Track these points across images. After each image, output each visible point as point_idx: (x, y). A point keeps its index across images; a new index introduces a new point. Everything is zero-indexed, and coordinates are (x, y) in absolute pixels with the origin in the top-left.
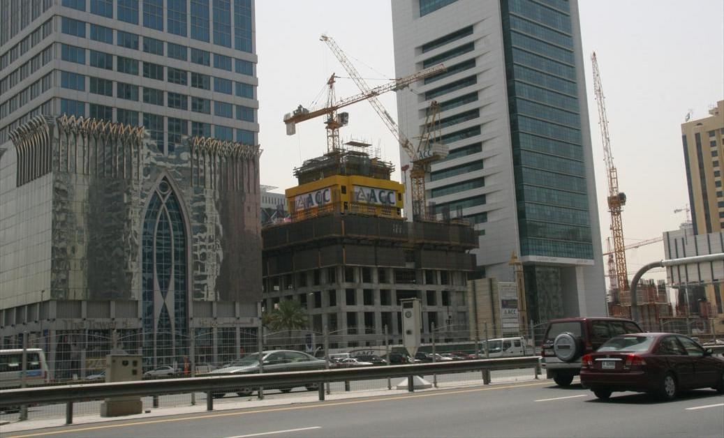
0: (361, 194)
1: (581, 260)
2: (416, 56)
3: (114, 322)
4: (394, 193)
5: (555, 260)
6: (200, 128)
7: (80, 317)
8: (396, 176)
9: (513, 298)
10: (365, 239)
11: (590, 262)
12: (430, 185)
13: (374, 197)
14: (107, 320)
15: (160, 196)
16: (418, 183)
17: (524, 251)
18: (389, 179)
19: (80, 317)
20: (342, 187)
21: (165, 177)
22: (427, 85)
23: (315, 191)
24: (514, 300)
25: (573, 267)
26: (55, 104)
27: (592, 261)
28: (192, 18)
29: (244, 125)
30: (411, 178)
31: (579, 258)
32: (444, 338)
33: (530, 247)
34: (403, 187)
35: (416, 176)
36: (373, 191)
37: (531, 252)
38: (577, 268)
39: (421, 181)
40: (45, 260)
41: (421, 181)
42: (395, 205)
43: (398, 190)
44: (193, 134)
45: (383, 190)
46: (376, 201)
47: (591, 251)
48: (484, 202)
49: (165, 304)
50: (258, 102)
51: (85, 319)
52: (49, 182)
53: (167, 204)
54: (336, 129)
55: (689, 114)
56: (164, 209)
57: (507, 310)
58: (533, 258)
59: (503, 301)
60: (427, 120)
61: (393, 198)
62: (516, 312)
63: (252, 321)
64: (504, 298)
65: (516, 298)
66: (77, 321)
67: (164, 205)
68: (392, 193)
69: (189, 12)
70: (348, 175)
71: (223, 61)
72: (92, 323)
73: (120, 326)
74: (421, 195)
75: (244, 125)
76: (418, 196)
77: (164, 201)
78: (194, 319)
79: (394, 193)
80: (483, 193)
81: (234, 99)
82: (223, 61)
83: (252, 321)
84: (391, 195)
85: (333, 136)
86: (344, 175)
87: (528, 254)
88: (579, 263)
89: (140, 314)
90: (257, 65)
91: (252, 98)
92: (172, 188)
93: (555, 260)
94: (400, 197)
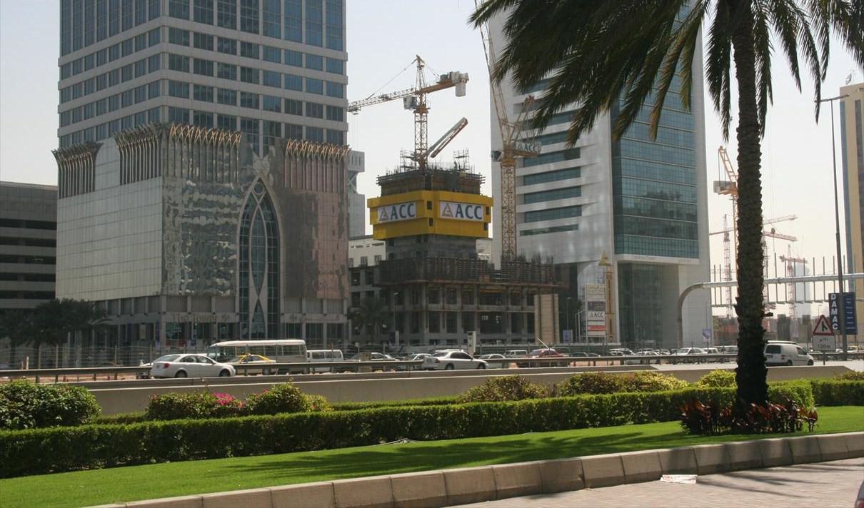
0: (448, 209)
1: (683, 259)
2: (514, 96)
3: (214, 316)
4: (482, 207)
5: (653, 258)
6: (294, 131)
7: (186, 311)
8: (486, 190)
9: (601, 300)
10: (450, 284)
11: (695, 261)
12: (522, 172)
13: (461, 212)
14: (209, 314)
15: (255, 197)
16: (508, 172)
17: (618, 249)
18: (478, 192)
19: (186, 311)
21: (260, 179)
22: (527, 186)
23: (399, 204)
24: (602, 302)
25: (677, 265)
26: (164, 85)
27: (697, 260)
28: (286, 18)
29: (334, 78)
30: (501, 167)
31: (681, 257)
32: (526, 338)
33: (626, 244)
34: (491, 200)
35: (506, 164)
36: (459, 207)
37: (626, 250)
38: (679, 267)
39: (512, 170)
40: (155, 258)
41: (512, 170)
43: (487, 205)
44: (286, 136)
46: (462, 216)
47: (696, 250)
48: (579, 194)
49: (259, 294)
50: (347, 54)
51: (190, 313)
52: (158, 185)
53: (262, 205)
54: (424, 114)
55: (851, 75)
56: (259, 209)
57: (594, 313)
58: (628, 257)
59: (589, 303)
60: (519, 118)
61: (481, 212)
62: (603, 314)
63: (338, 317)
64: (590, 300)
65: (604, 300)
66: (183, 314)
67: (259, 206)
68: (480, 207)
69: (283, 12)
70: (436, 189)
71: (314, 62)
72: (196, 316)
73: (220, 320)
74: (512, 185)
75: (334, 78)
76: (508, 186)
77: (259, 202)
78: (285, 314)
80: (578, 165)
81: (324, 75)
82: (314, 62)
83: (338, 317)
84: (478, 209)
85: (421, 122)
86: (430, 189)
87: (623, 253)
88: (681, 263)
89: (237, 310)
90: (347, 86)
91: (342, 50)
92: (266, 189)
93: (653, 258)
94: (488, 211)
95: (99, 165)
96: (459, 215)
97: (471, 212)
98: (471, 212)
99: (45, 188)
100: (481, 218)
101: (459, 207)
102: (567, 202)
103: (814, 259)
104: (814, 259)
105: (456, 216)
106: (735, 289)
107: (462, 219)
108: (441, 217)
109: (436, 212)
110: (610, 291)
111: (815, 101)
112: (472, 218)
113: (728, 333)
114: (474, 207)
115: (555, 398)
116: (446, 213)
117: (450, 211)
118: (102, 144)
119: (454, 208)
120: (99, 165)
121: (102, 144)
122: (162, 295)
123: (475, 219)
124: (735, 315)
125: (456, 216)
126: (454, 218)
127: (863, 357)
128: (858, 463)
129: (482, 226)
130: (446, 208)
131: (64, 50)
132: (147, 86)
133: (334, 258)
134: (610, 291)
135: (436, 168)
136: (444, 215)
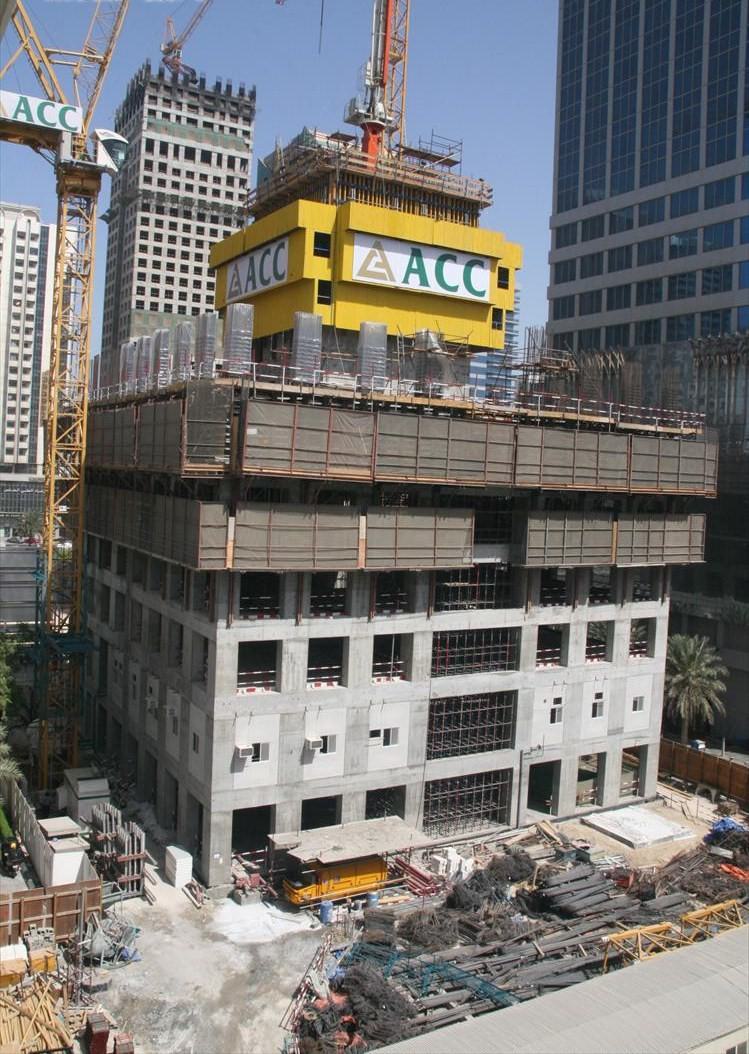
13: (421, 271)
42: (485, 299)
45: (448, 254)
46: (424, 282)
79: (487, 263)
95: (744, 1027)
98: (454, 272)
99: (344, 646)
100: (482, 294)
105: (406, 281)
107: (424, 289)
109: (336, 266)
110: (571, 881)
111: (72, 1048)
112: (455, 289)
113: (100, 567)
116: (371, 267)
117: (385, 264)
120: (744, 1027)
122: (155, 493)
124: (747, 828)
125: (406, 281)
126: (398, 283)
127: (742, 785)
131: (564, 199)
132: (580, 224)
133: (411, 839)
134: (571, 881)
136: (363, 271)
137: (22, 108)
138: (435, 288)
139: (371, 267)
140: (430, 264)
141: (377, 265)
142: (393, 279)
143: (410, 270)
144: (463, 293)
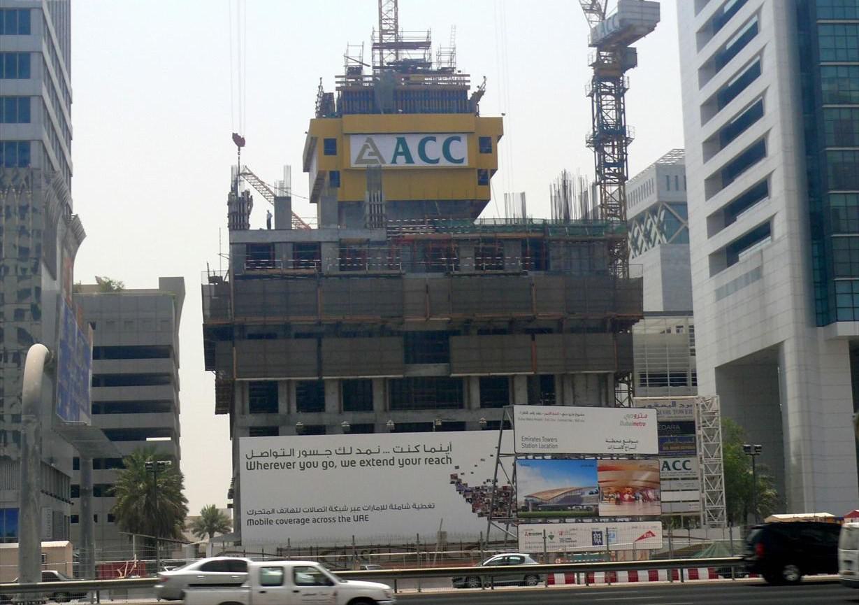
20: (326, 141)
36: (402, 142)
42: (465, 164)
46: (409, 160)
84: (454, 144)
96: (401, 161)
97: (434, 150)
98: (434, 150)
101: (402, 142)
102: (402, 601)
103: (442, 520)
104: (442, 520)
105: (394, 161)
106: (857, 297)
108: (353, 165)
112: (437, 161)
114: (441, 140)
115: (4, 164)
116: (366, 156)
117: (376, 152)
118: (697, 13)
119: (387, 147)
121: (697, 13)
123: (444, 163)
125: (394, 161)
126: (388, 164)
128: (855, 303)
129: (474, 177)
130: (366, 147)
135: (455, 534)
136: (360, 160)
137: (401, 150)
138: (418, 162)
139: (366, 156)
140: (413, 144)
141: (371, 154)
142: (384, 162)
143: (397, 153)
144: (444, 163)
